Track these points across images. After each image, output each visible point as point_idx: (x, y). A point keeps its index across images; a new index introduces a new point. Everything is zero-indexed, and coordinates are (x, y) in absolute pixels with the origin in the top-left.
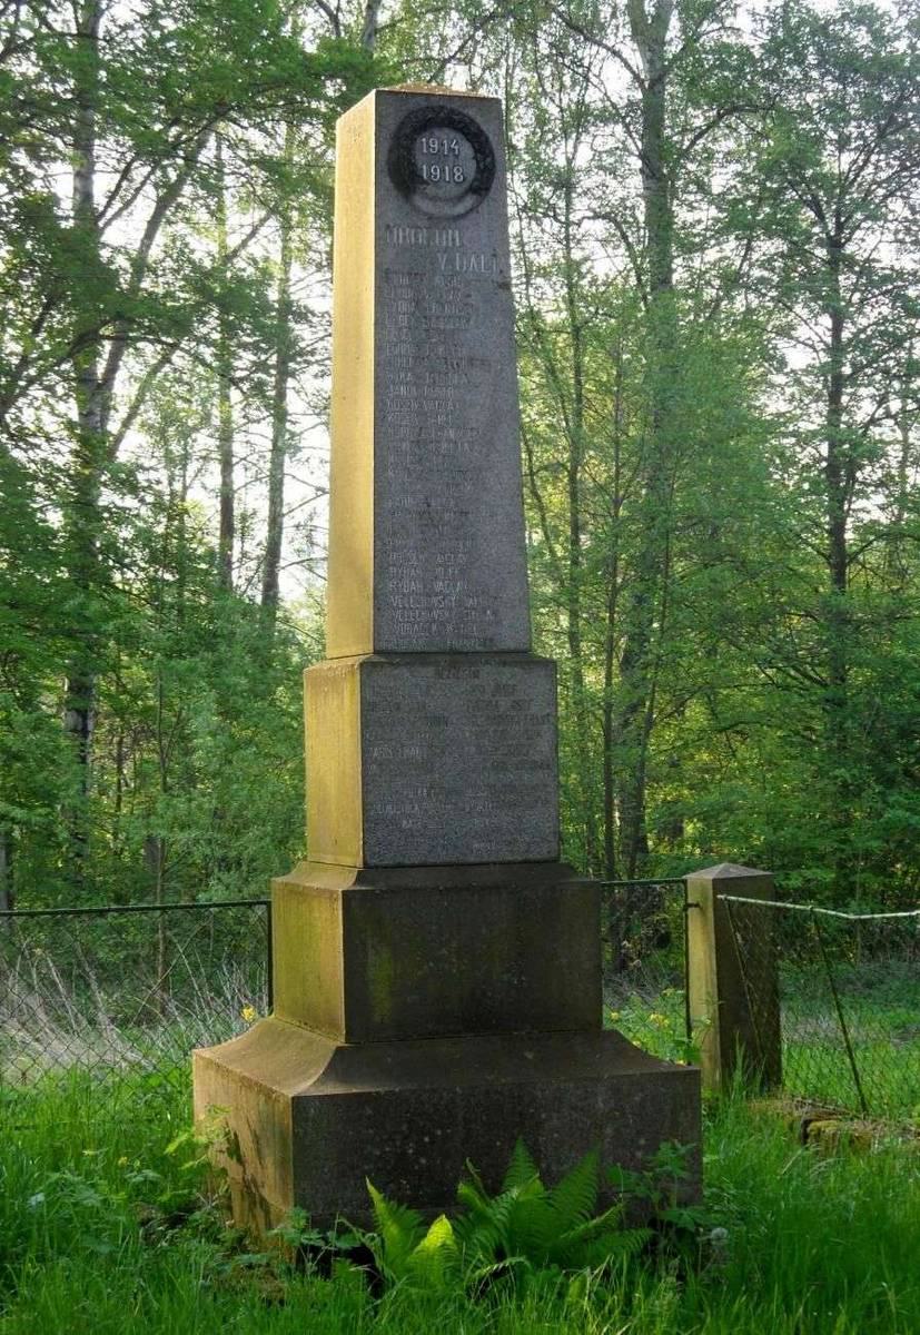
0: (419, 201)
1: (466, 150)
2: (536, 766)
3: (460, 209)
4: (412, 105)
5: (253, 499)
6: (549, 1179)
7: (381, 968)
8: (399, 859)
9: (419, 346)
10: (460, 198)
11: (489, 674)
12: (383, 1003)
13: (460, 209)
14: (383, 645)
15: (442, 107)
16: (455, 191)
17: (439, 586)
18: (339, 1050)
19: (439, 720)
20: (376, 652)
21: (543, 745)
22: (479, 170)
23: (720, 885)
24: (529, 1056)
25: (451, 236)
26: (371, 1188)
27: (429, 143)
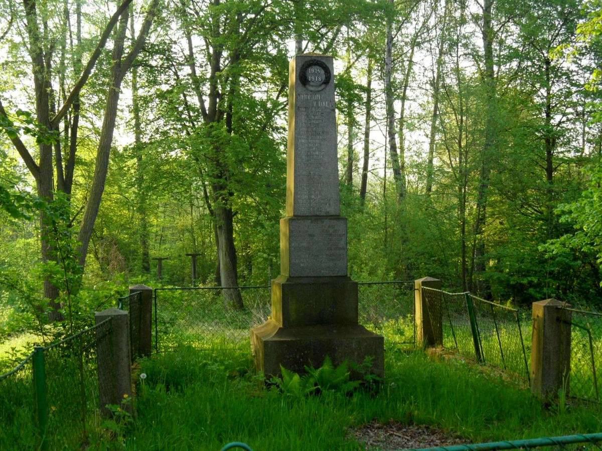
0: (307, 86)
1: (323, 72)
2: (340, 249)
3: (320, 89)
4: (307, 59)
5: (359, 147)
6: (335, 366)
7: (293, 307)
8: (300, 275)
9: (308, 128)
10: (320, 85)
11: (327, 222)
12: (293, 316)
13: (320, 89)
14: (296, 214)
15: (315, 60)
16: (319, 83)
17: (313, 197)
18: (280, 328)
19: (311, 236)
20: (294, 216)
21: (342, 243)
22: (326, 78)
23: (424, 283)
24: (335, 331)
25: (318, 96)
26: (281, 366)
27: (312, 70)
